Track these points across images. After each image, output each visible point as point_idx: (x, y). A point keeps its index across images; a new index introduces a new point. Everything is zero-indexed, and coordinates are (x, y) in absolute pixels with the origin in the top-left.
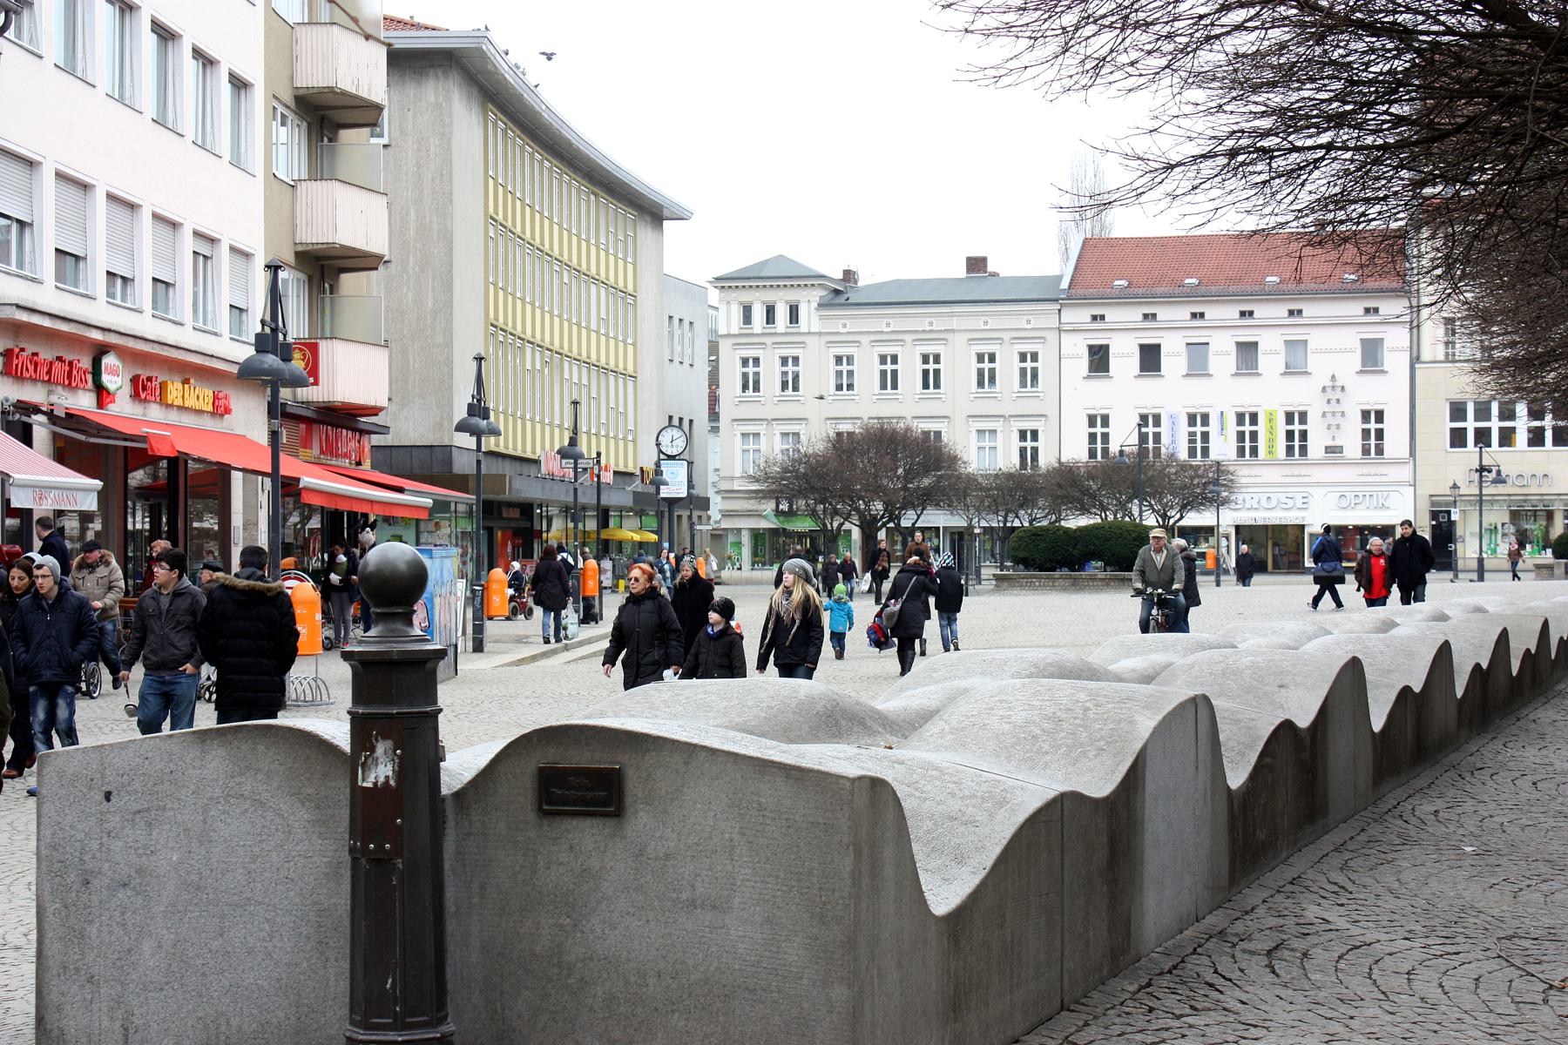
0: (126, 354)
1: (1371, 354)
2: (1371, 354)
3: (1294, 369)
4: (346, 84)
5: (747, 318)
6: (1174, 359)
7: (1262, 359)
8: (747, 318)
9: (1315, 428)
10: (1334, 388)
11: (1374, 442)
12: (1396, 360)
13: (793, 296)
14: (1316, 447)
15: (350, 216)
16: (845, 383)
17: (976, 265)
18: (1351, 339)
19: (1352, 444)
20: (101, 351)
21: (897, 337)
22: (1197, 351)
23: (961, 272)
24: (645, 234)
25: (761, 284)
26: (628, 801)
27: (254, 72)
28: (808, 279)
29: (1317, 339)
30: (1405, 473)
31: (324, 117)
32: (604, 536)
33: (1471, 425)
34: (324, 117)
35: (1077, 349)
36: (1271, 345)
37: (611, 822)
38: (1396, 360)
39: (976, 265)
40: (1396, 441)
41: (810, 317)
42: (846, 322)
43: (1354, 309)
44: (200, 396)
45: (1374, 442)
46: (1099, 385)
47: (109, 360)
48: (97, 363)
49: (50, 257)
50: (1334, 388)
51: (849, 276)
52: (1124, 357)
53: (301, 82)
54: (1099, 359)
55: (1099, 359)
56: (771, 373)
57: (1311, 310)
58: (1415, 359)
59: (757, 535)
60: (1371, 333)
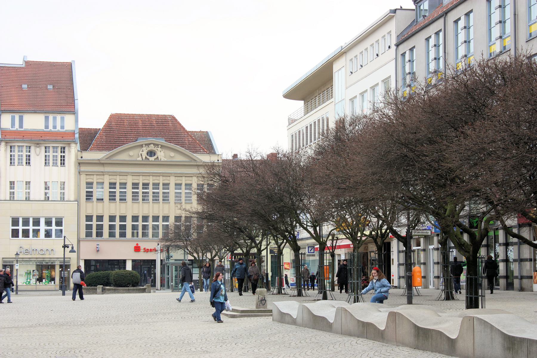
33: (21, 228)
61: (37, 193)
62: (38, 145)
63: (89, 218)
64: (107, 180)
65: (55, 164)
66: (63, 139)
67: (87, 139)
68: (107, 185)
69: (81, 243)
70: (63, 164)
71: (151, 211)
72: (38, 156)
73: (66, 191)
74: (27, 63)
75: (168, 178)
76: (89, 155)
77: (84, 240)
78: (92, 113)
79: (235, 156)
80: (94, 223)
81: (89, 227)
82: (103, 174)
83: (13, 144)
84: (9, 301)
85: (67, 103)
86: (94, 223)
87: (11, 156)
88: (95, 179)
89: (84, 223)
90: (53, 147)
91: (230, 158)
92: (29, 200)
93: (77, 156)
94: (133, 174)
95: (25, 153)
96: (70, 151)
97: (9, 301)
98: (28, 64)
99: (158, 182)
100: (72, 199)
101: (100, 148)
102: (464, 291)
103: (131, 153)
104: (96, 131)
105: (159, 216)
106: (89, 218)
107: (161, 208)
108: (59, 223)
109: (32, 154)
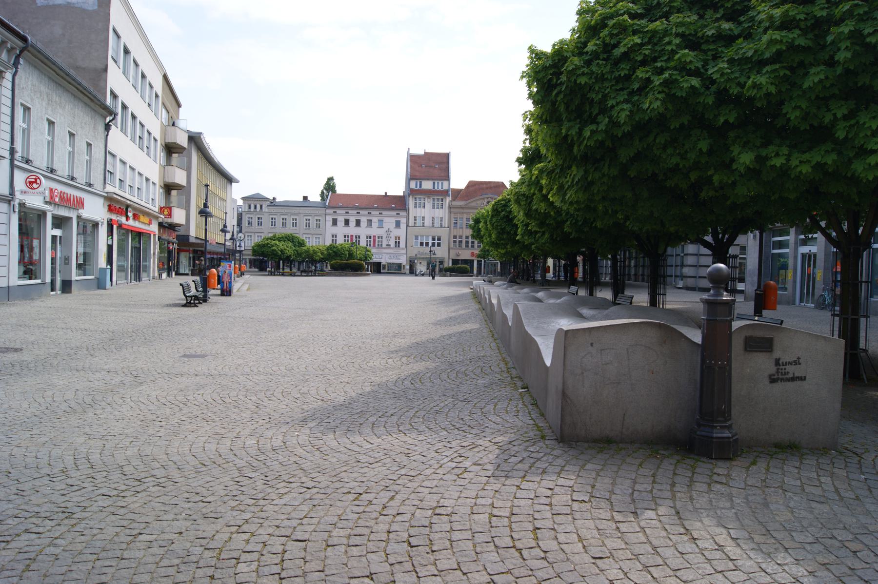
0: (134, 209)
1: (398, 224)
2: (398, 224)
3: (381, 226)
4: (178, 142)
5: (250, 207)
6: (364, 223)
7: (338, 223)
8: (250, 207)
9: (384, 240)
10: (388, 231)
11: (397, 244)
12: (403, 226)
13: (261, 203)
14: (384, 245)
15: (179, 177)
16: (273, 224)
17: (305, 198)
18: (393, 220)
19: (393, 245)
20: (128, 206)
21: (286, 214)
22: (370, 222)
23: (302, 200)
24: (229, 186)
25: (254, 201)
26: (775, 347)
27: (158, 138)
28: (266, 199)
29: (386, 220)
30: (404, 251)
31: (170, 149)
32: (248, 256)
33: (436, 242)
34: (170, 149)
35: (329, 219)
36: (375, 220)
37: (768, 354)
38: (403, 226)
39: (305, 198)
40: (403, 245)
41: (265, 209)
42: (274, 210)
43: (394, 213)
44: (145, 219)
45: (397, 244)
46: (334, 228)
47: (129, 209)
48: (127, 209)
49: (118, 181)
50: (388, 231)
51: (274, 199)
52: (352, 223)
53: (167, 141)
54: (335, 222)
55: (335, 222)
56: (255, 221)
57: (384, 213)
58: (408, 226)
59: (250, 260)
60: (398, 219)
61: (428, 222)
62: (429, 197)
63: (455, 237)
64: (465, 216)
65: (438, 208)
66: (445, 193)
67: (457, 193)
72: (429, 203)
76: (455, 203)
78: (458, 181)
81: (455, 242)
82: (463, 213)
84: (797, 362)
85: (445, 176)
86: (458, 240)
88: (459, 216)
89: (452, 240)
97: (797, 362)
98: (426, 153)
101: (462, 199)
102: (17, 213)
104: (461, 190)
106: (455, 237)
108: (439, 239)
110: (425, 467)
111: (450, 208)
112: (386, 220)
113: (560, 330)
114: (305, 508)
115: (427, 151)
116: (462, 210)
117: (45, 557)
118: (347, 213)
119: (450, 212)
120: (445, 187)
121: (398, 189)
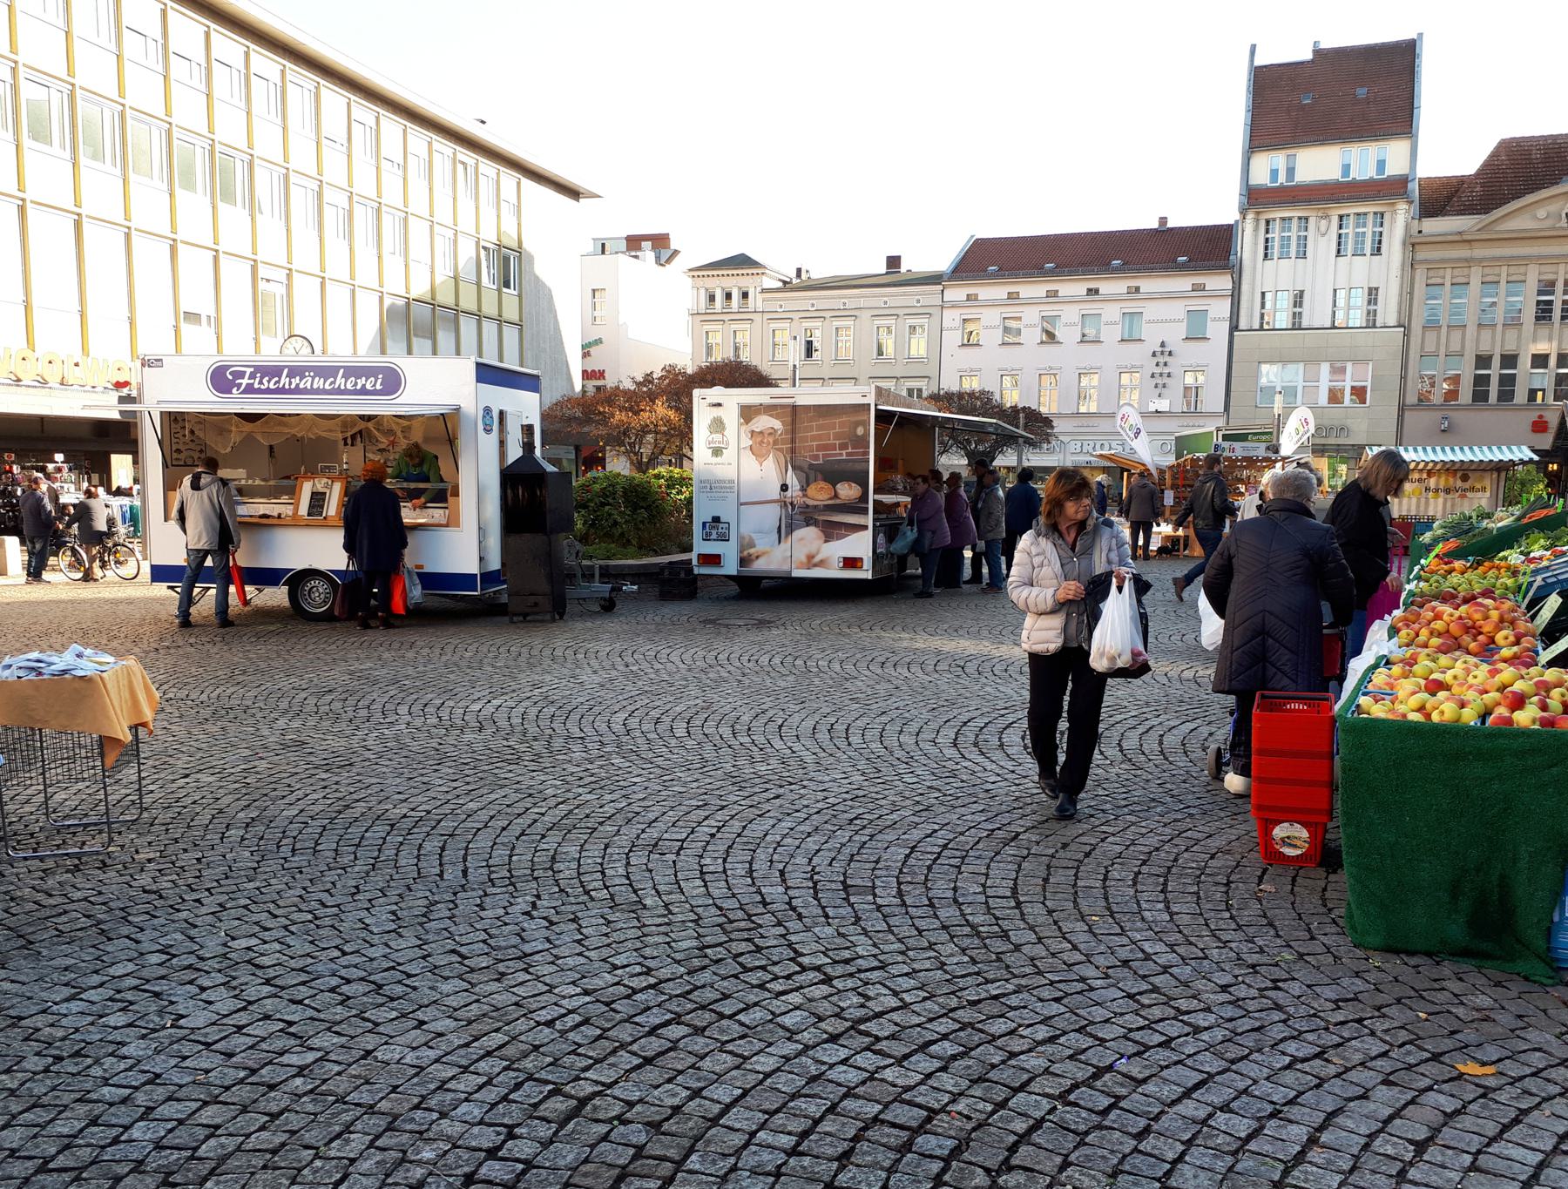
5: (712, 298)
23: (882, 268)
39: (893, 262)
43: (1183, 283)
58: (1234, 328)
68: (1532, 285)
69: (1407, 414)
70: (1377, 251)
71: (1498, 344)
72: (1322, 236)
73: (1380, 308)
74: (1318, 53)
75: (1522, 269)
76: (1434, 226)
77: (1414, 407)
78: (1452, 137)
79: (1163, 220)
80: (1495, 371)
83: (1271, 216)
87: (1267, 240)
90: (1283, 219)
91: (1155, 225)
92: (1374, 326)
93: (1407, 227)
94: (1540, 260)
95: (1369, 230)
96: (1393, 221)
99: (1551, 277)
100: (1392, 321)
103: (1541, 213)
105: (1491, 357)
107: (1443, 340)
109: (1311, 234)
110: (973, 953)
111: (1412, 244)
112: (1151, 310)
113: (1034, 658)
114: (1219, 1034)
115: (1326, 44)
116: (1463, 252)
117: (307, 844)
118: (1198, 288)
119: (1411, 265)
120: (1395, 168)
121: (1210, 201)
